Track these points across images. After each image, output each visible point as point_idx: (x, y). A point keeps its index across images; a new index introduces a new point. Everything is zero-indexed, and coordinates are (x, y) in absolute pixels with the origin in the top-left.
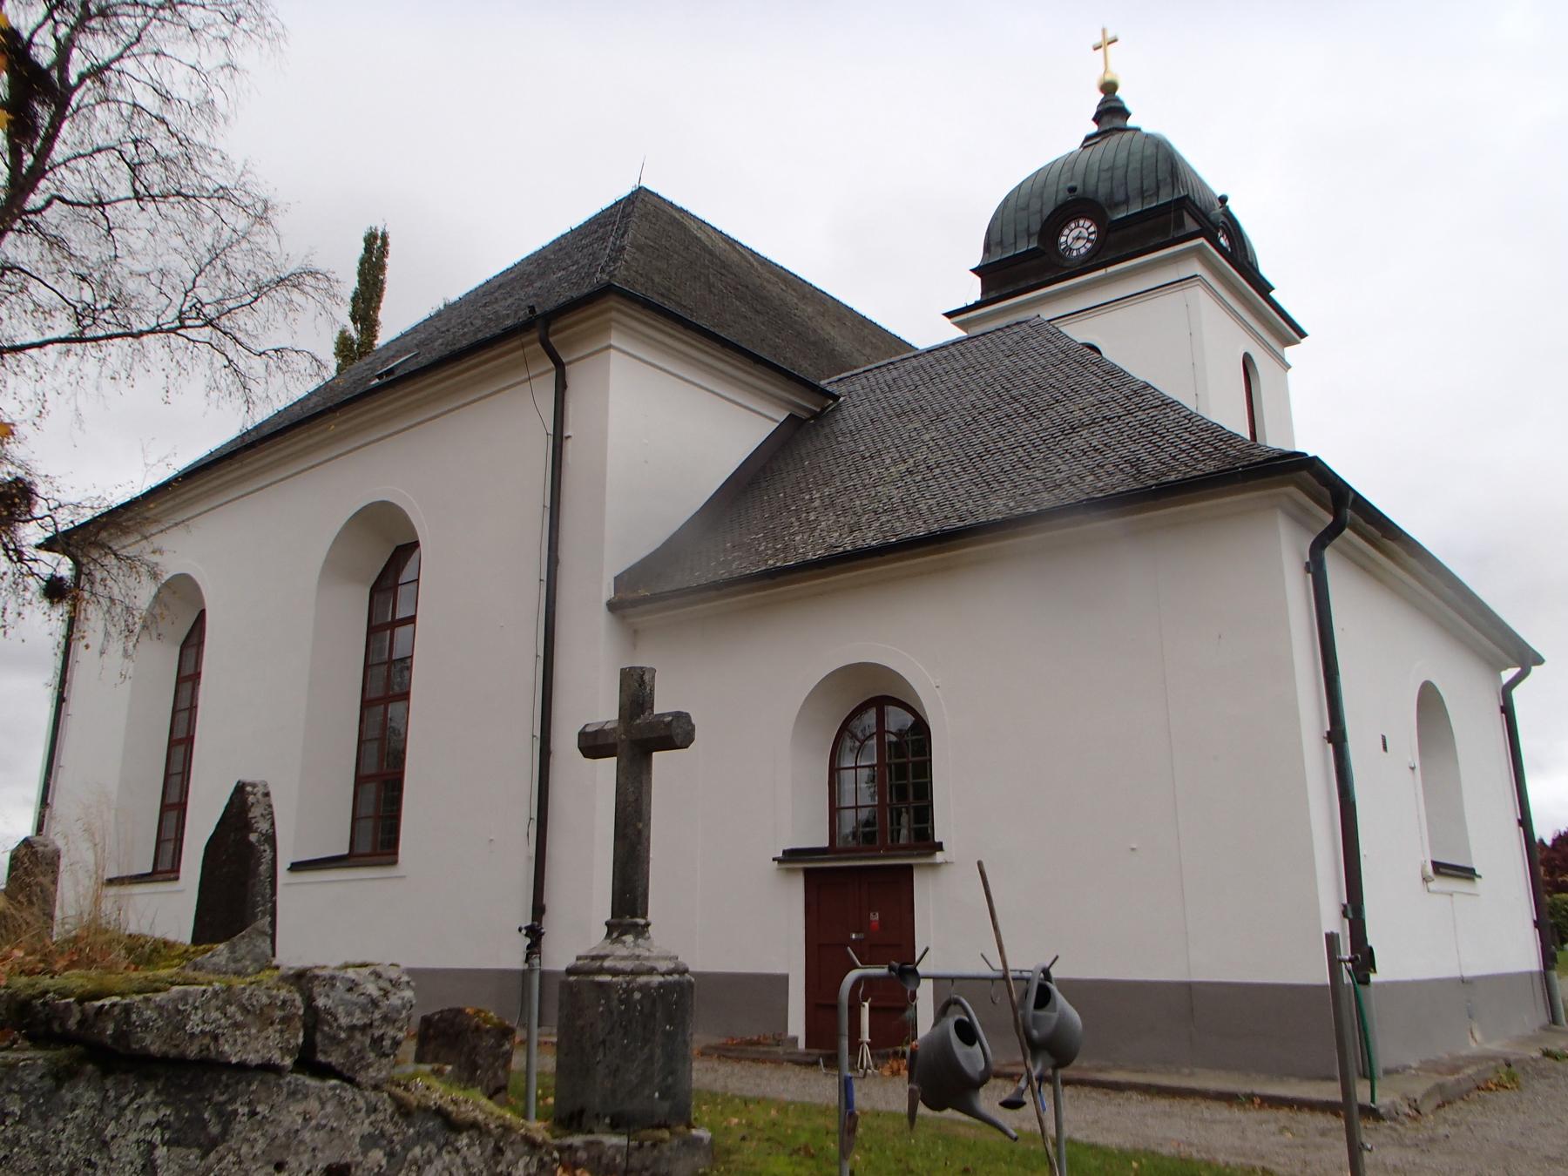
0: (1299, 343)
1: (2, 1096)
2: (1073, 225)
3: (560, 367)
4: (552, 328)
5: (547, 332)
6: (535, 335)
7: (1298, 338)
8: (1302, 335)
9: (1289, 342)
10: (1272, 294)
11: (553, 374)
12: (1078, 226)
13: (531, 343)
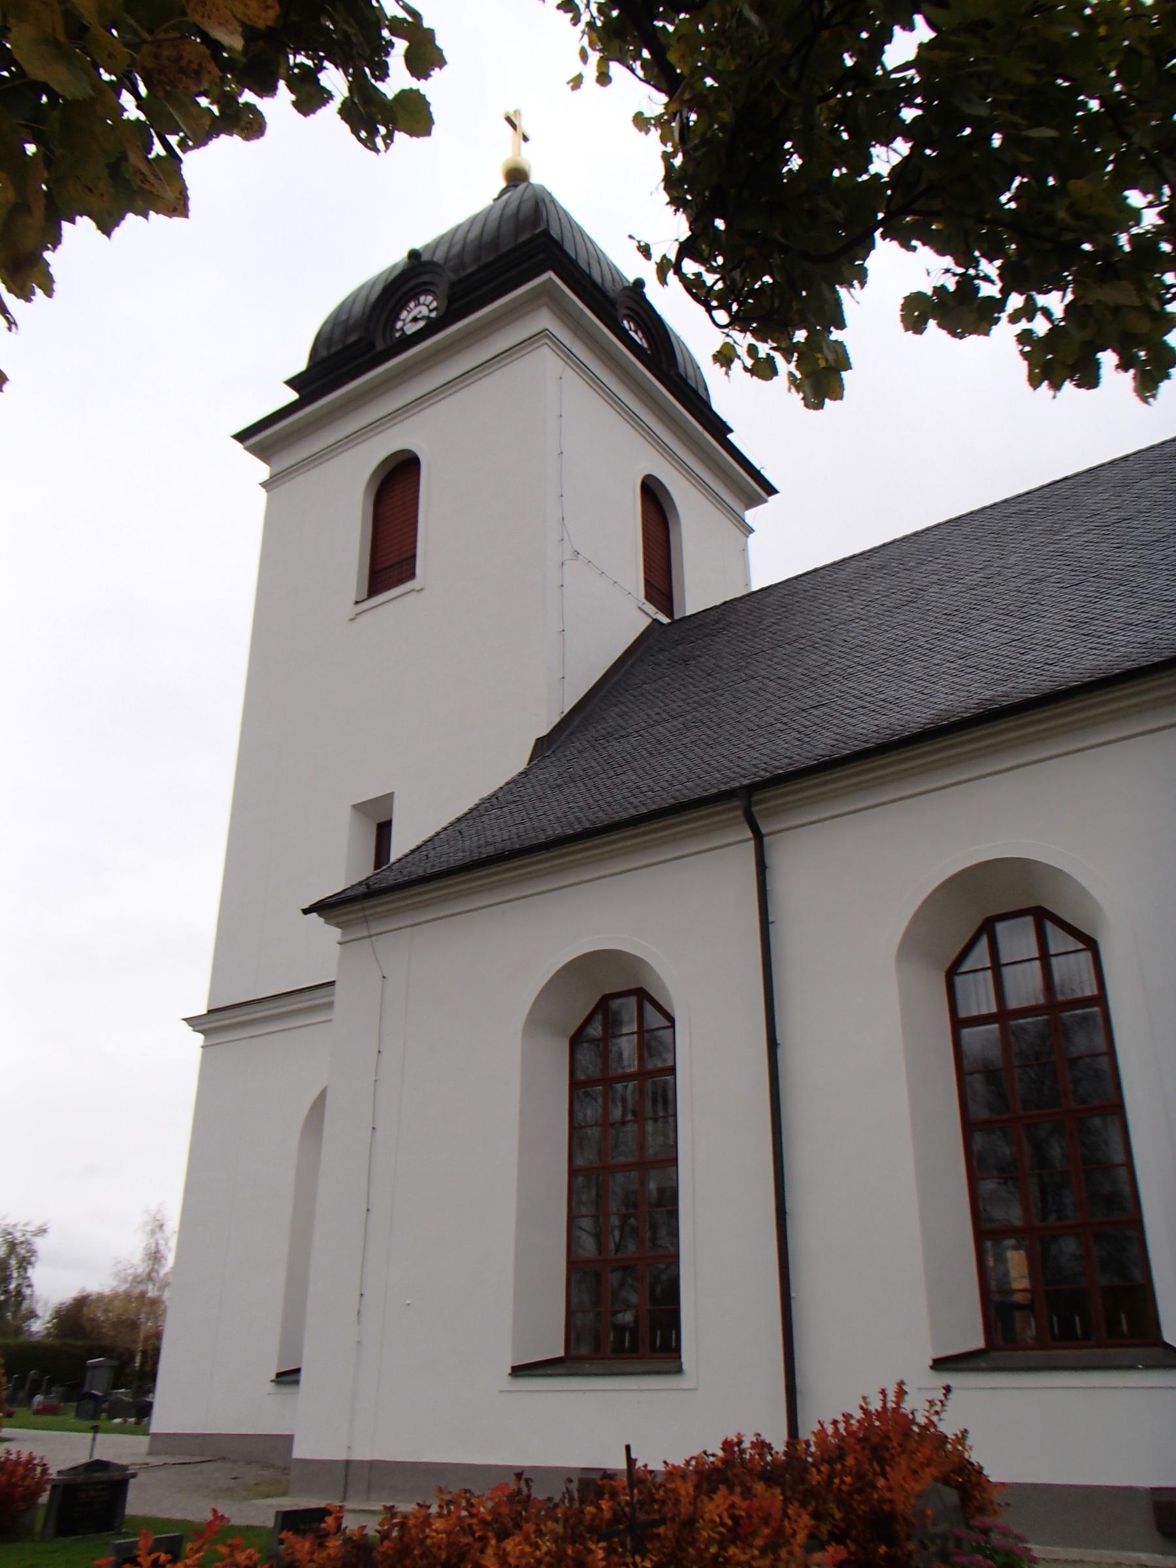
0: (766, 501)
1: (128, 1556)
2: (412, 305)
3: (758, 837)
4: (755, 798)
5: (750, 802)
6: (737, 803)
7: (763, 494)
8: (771, 490)
9: (753, 501)
10: (730, 436)
11: (752, 843)
12: (419, 304)
13: (735, 809)
